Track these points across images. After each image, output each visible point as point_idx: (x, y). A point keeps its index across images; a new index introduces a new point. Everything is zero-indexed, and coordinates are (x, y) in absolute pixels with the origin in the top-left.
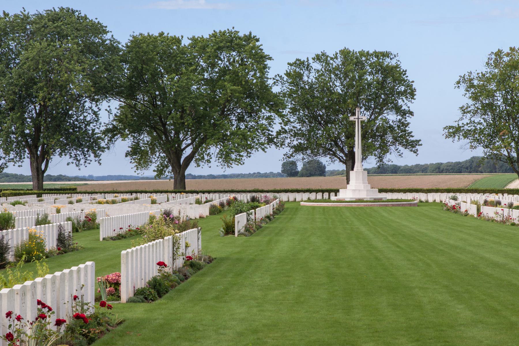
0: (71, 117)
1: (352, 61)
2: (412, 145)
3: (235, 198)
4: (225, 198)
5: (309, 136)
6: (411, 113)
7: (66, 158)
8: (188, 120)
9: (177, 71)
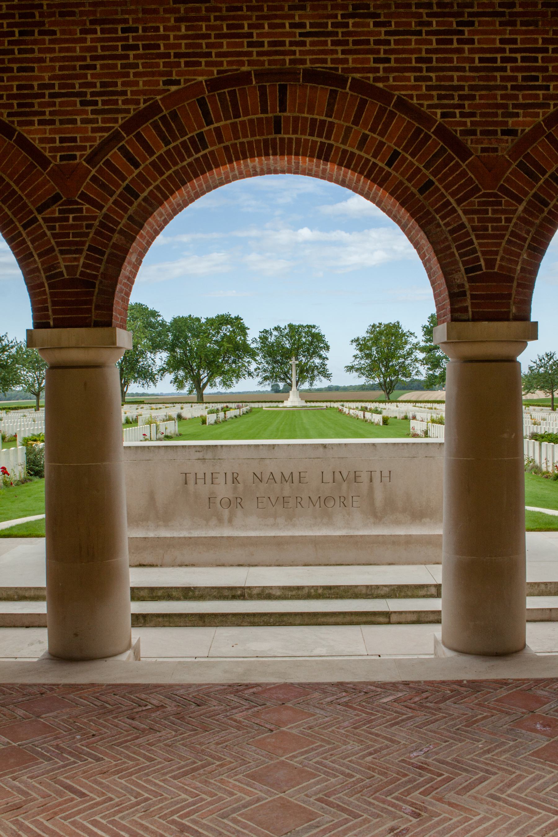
0: (139, 362)
2: (328, 376)
3: (227, 407)
4: (225, 405)
5: (272, 372)
6: (327, 359)
7: (136, 384)
8: (204, 364)
9: (198, 337)
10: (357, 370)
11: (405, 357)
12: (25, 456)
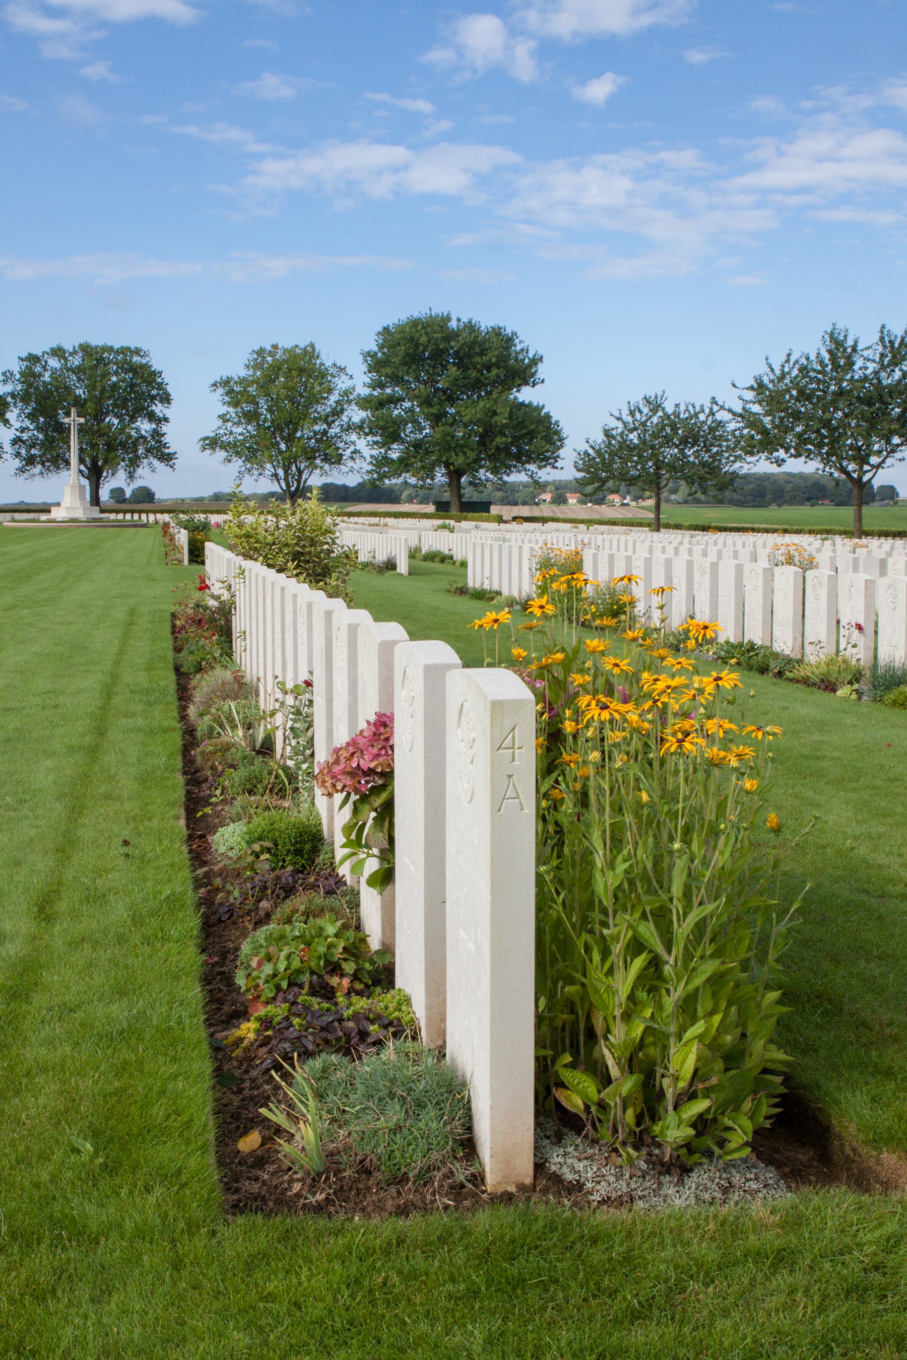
1: (95, 358)
6: (166, 420)
10: (224, 447)
11: (328, 420)
12: (752, 674)
